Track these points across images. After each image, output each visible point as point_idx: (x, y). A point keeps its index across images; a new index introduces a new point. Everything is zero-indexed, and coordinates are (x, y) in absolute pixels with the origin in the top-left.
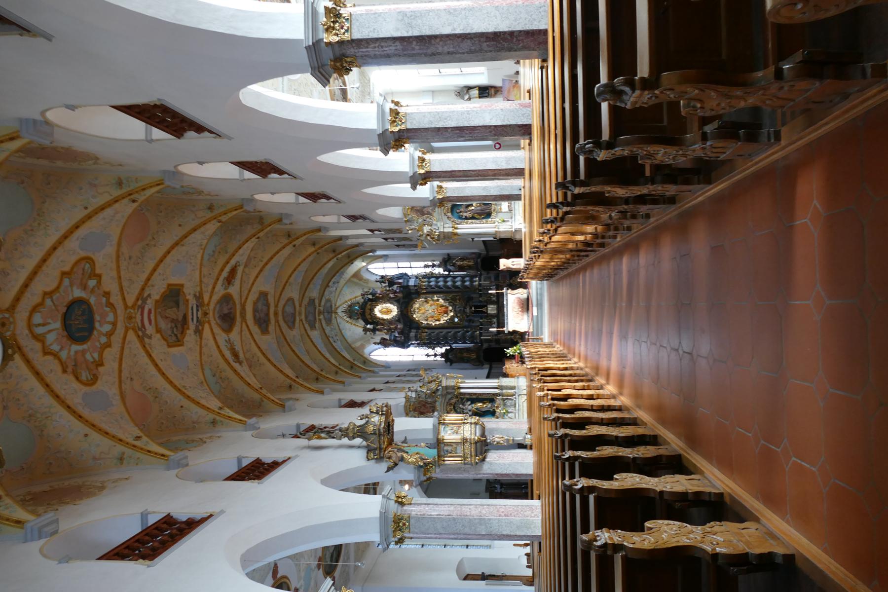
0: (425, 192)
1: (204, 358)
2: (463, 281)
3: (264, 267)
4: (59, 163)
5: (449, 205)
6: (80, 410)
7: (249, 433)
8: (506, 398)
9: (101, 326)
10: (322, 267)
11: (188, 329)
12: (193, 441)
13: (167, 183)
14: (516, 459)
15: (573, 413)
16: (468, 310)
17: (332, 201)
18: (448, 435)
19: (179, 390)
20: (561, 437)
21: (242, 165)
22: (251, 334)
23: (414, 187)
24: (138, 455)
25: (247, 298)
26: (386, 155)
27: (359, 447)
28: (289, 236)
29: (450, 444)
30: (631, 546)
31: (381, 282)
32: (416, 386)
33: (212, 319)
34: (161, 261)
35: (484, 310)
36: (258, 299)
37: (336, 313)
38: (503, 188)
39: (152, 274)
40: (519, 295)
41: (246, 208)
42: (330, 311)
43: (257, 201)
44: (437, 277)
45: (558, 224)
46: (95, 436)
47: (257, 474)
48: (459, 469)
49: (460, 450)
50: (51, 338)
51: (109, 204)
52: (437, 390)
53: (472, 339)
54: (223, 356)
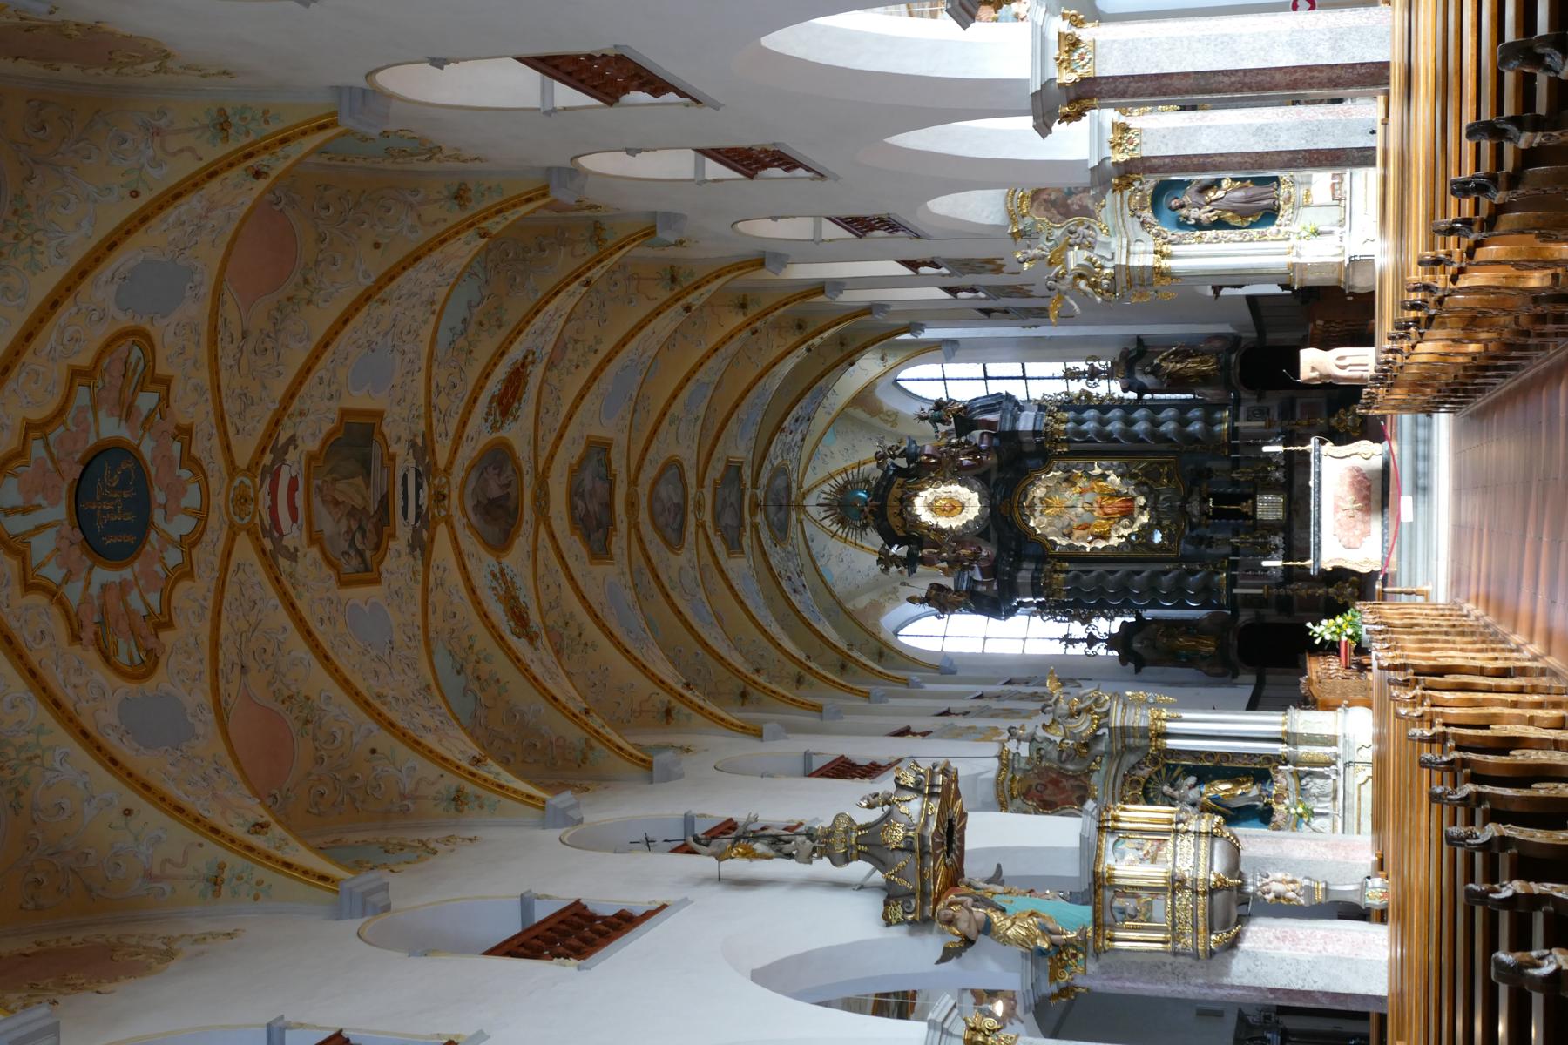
0: (1076, 143)
1: (435, 621)
2: (1183, 422)
3: (601, 368)
4: (68, 71)
5: (1150, 182)
6: (112, 741)
7: (555, 833)
8: (1307, 771)
9: (168, 518)
10: (767, 370)
11: (393, 536)
12: (402, 847)
13: (346, 122)
14: (1334, 949)
15: (1528, 787)
16: (1194, 507)
17: (800, 172)
18: (1128, 865)
19: (366, 705)
20: (1486, 847)
21: (553, 66)
22: (561, 558)
23: (1043, 128)
24: (260, 872)
25: (551, 457)
26: (965, 25)
27: (862, 887)
28: (673, 279)
29: (1132, 891)
31: (935, 421)
32: (1033, 726)
33: (457, 514)
34: (325, 345)
35: (1245, 507)
36: (583, 460)
37: (801, 507)
39: (299, 381)
40: (1358, 462)
41: (557, 194)
42: (783, 504)
44: (1104, 406)
45: (1500, 197)
46: (151, 817)
47: (574, 941)
48: (1158, 966)
49: (1161, 907)
50: (42, 546)
51: (194, 183)
52: (1095, 738)
53: (1206, 595)
54: (485, 616)
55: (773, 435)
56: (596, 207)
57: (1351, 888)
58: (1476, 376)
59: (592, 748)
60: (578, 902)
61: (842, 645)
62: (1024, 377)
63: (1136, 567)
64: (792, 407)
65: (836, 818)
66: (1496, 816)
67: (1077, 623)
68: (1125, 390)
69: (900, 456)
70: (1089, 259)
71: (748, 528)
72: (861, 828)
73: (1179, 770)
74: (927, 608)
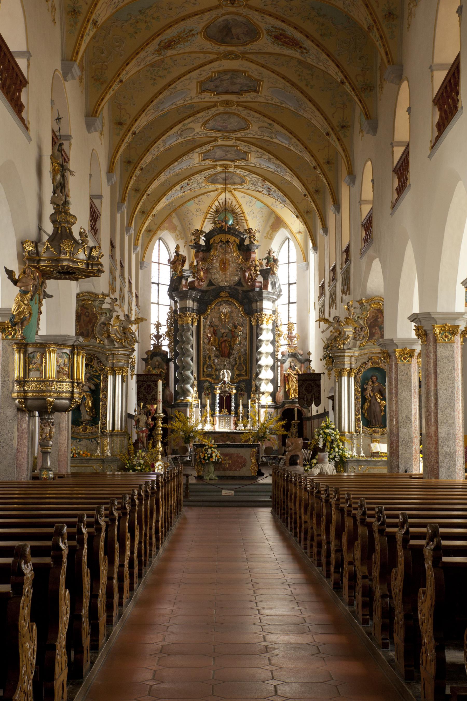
3: (298, 88)
7: (58, 65)
17: (396, 196)
20: (97, 522)
21: (454, 73)
23: (414, 318)
26: (462, 283)
28: (343, 127)
30: (21, 605)
31: (268, 259)
37: (225, 190)
38: (408, 445)
42: (228, 182)
43: (399, 85)
47: (8, 82)
55: (261, 176)
56: (382, 87)
57: (49, 464)
58: (291, 518)
59: (102, 84)
60: (27, 82)
61: (154, 212)
62: (289, 303)
63: (195, 359)
64: (276, 186)
65: (74, 216)
66: (109, 527)
67: (166, 330)
68: (282, 353)
69: (251, 241)
70: (348, 337)
71: (214, 163)
72: (70, 229)
73: (98, 381)
74: (173, 255)
